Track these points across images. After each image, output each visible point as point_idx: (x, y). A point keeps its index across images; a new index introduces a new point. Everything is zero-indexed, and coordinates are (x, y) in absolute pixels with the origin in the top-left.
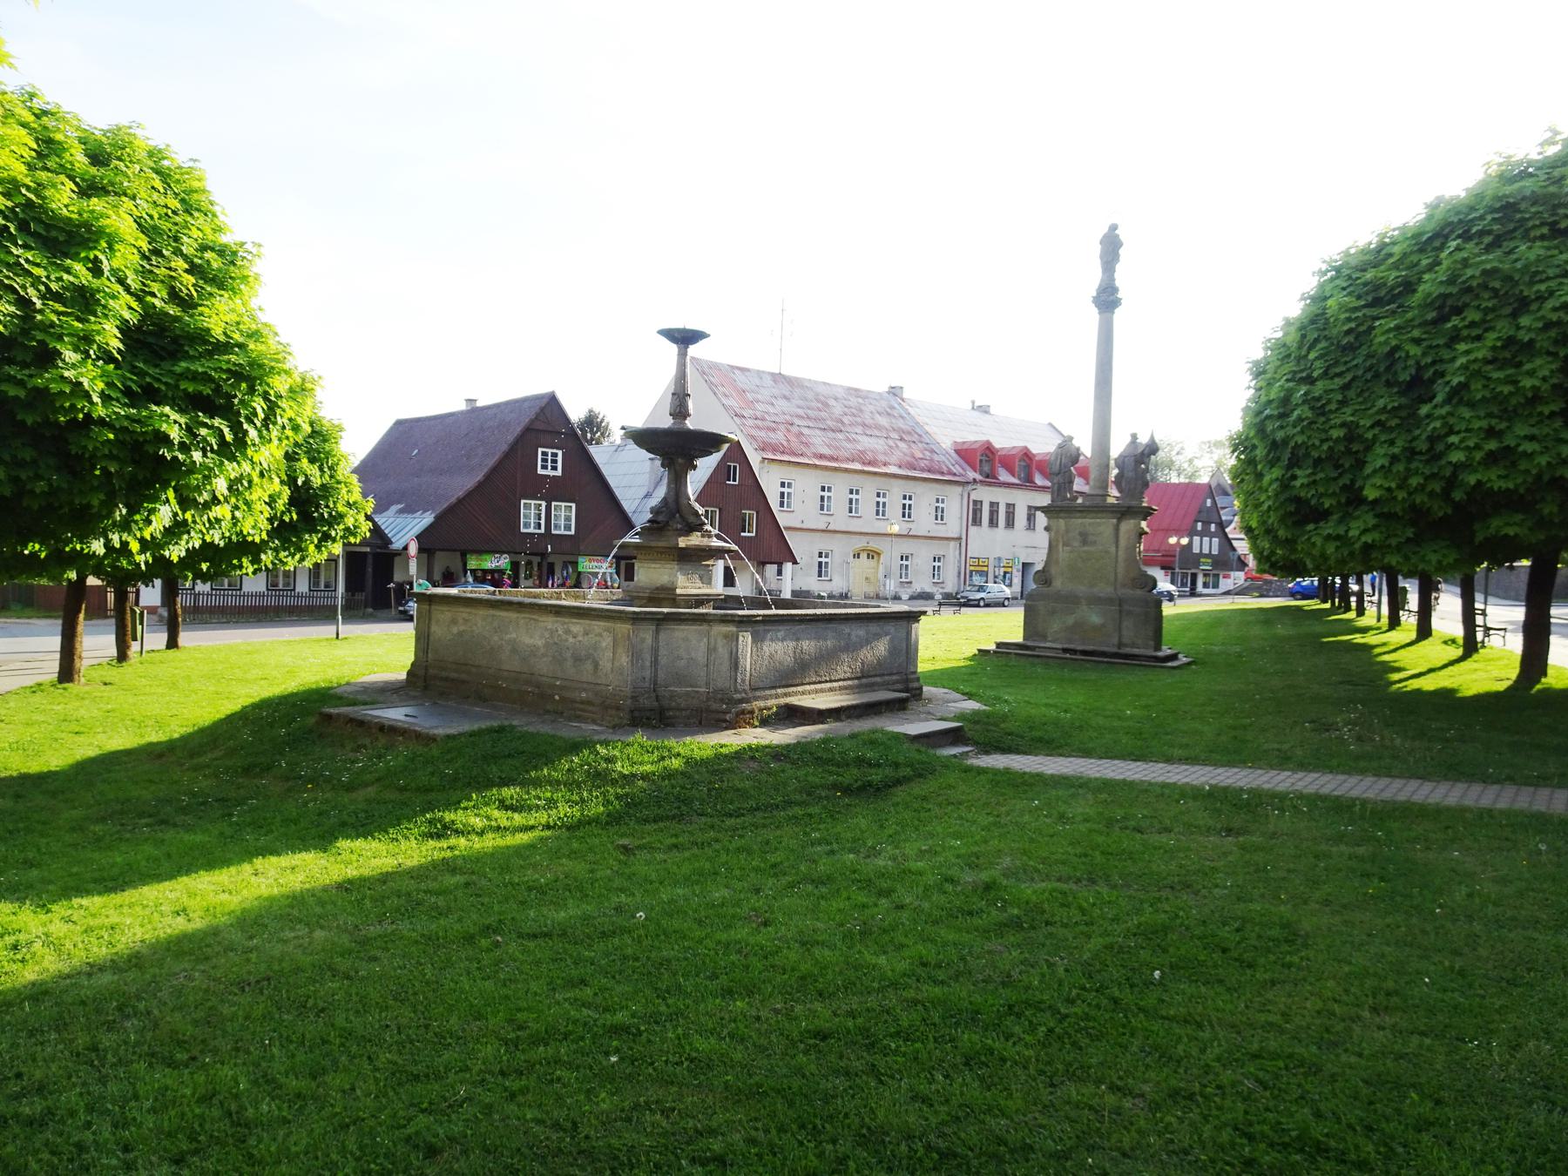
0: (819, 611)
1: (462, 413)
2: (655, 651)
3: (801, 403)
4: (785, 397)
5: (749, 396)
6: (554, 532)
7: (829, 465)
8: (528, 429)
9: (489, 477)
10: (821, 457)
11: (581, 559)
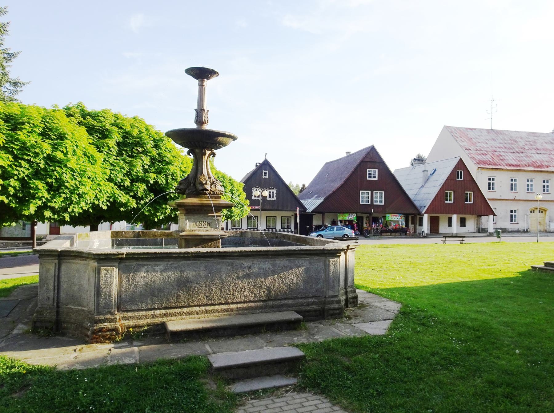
0: (294, 248)
1: (344, 158)
2: (58, 278)
3: (502, 141)
4: (493, 140)
5: (474, 141)
6: (374, 204)
7: (516, 168)
8: (362, 162)
9: (346, 182)
10: (511, 165)
11: (387, 215)
